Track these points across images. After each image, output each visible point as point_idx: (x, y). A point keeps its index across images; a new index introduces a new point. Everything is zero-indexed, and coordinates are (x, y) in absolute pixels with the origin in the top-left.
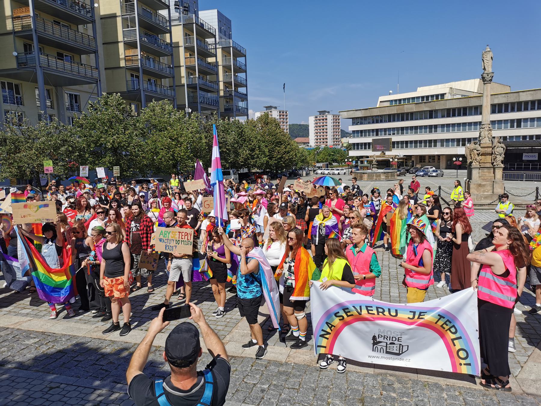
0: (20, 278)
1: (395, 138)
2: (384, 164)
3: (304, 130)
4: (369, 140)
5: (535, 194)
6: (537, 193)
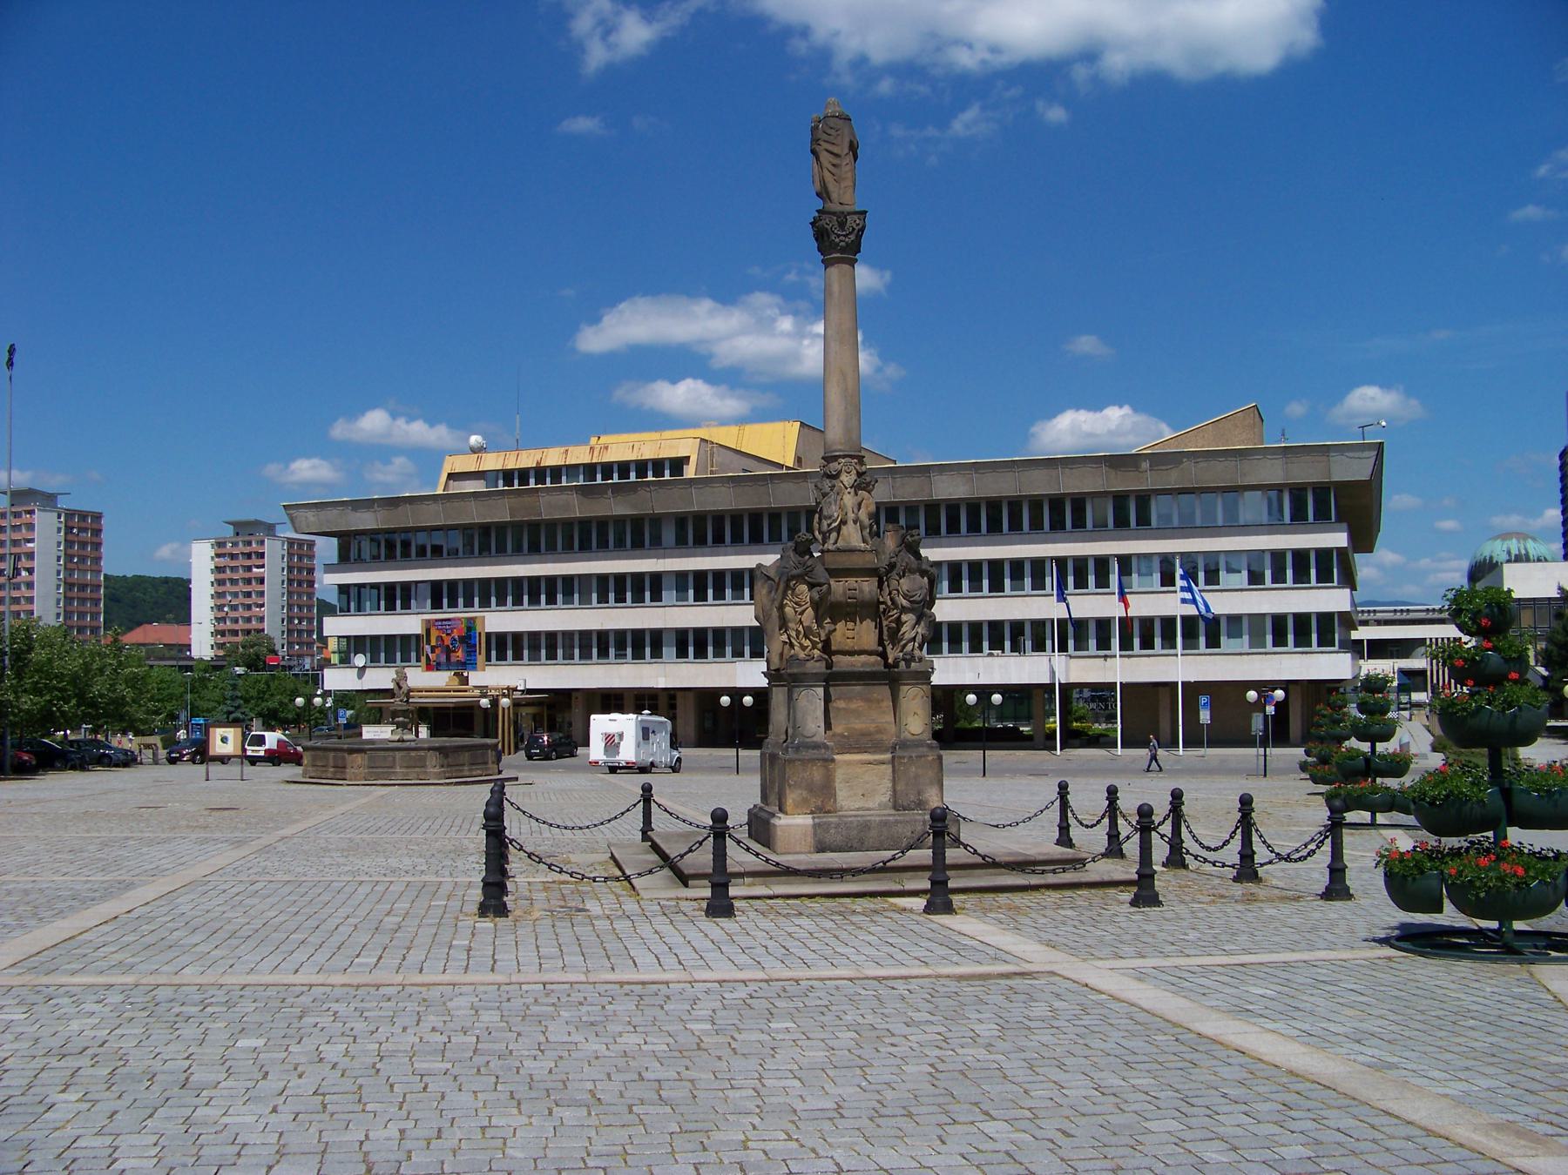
0: (1425, 756)
1: (499, 620)
2: (454, 719)
3: (172, 598)
4: (408, 624)
5: (1054, 814)
6: (1064, 806)
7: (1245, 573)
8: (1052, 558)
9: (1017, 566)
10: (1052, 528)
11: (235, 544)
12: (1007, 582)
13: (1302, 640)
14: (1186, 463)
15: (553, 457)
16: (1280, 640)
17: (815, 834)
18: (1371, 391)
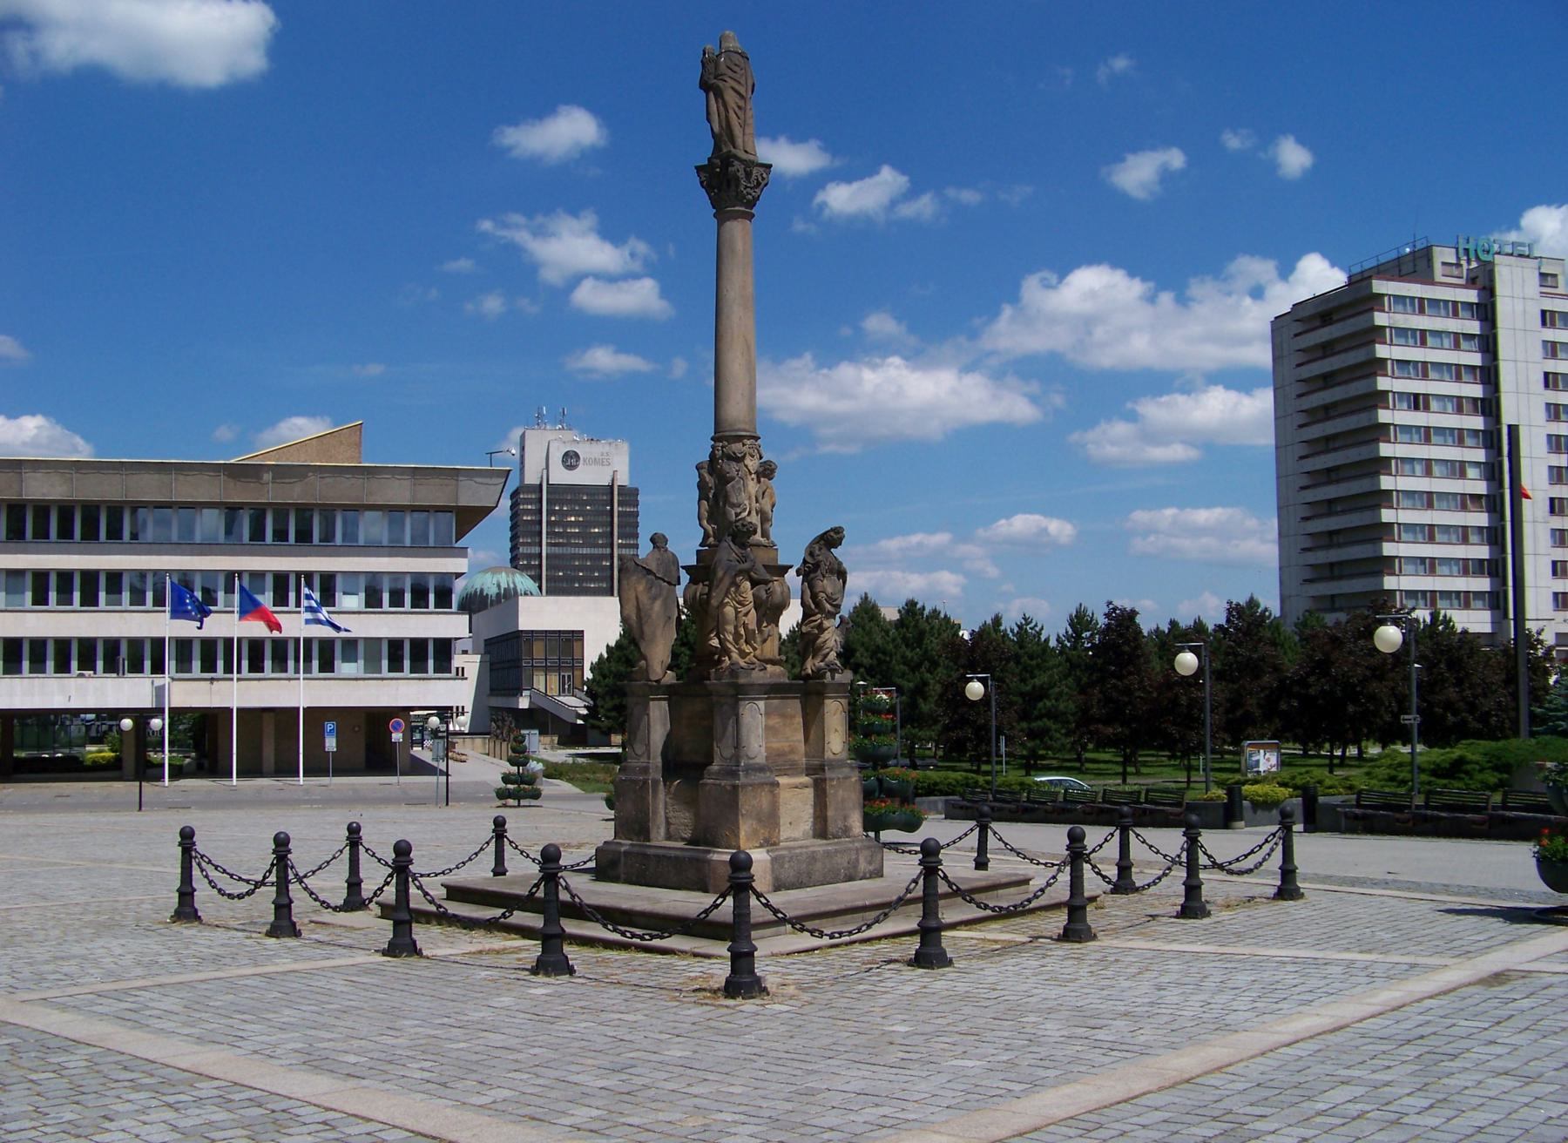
7: (363, 595)
9: (115, 578)
10: (36, 536)
12: (102, 595)
13: (419, 666)
14: (312, 478)
16: (395, 665)
17: (773, 870)
18: (300, 421)
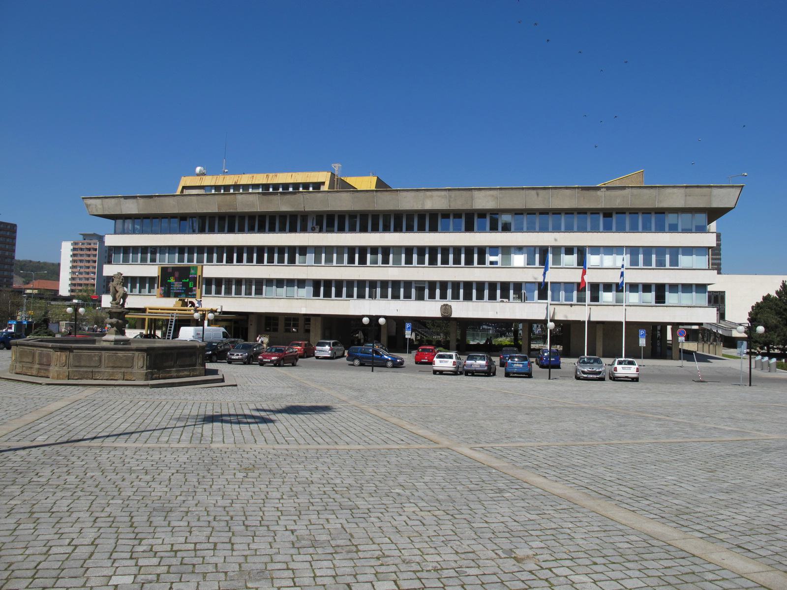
1: (212, 271)
8: (551, 246)
11: (83, 244)
15: (245, 179)
